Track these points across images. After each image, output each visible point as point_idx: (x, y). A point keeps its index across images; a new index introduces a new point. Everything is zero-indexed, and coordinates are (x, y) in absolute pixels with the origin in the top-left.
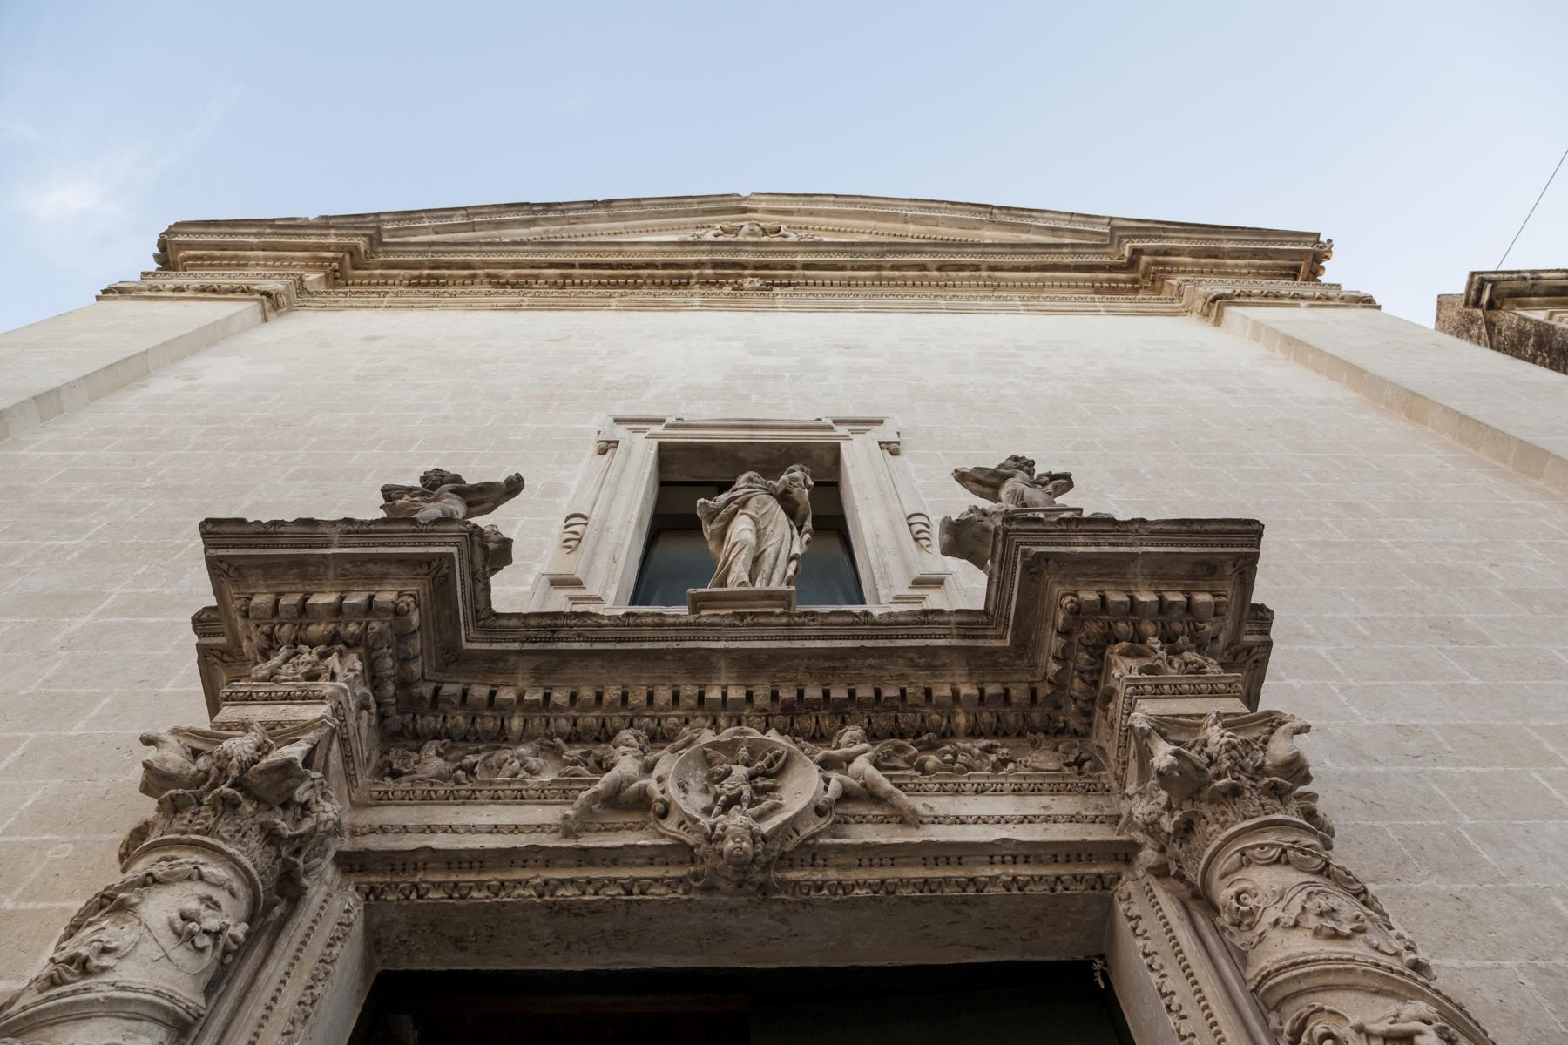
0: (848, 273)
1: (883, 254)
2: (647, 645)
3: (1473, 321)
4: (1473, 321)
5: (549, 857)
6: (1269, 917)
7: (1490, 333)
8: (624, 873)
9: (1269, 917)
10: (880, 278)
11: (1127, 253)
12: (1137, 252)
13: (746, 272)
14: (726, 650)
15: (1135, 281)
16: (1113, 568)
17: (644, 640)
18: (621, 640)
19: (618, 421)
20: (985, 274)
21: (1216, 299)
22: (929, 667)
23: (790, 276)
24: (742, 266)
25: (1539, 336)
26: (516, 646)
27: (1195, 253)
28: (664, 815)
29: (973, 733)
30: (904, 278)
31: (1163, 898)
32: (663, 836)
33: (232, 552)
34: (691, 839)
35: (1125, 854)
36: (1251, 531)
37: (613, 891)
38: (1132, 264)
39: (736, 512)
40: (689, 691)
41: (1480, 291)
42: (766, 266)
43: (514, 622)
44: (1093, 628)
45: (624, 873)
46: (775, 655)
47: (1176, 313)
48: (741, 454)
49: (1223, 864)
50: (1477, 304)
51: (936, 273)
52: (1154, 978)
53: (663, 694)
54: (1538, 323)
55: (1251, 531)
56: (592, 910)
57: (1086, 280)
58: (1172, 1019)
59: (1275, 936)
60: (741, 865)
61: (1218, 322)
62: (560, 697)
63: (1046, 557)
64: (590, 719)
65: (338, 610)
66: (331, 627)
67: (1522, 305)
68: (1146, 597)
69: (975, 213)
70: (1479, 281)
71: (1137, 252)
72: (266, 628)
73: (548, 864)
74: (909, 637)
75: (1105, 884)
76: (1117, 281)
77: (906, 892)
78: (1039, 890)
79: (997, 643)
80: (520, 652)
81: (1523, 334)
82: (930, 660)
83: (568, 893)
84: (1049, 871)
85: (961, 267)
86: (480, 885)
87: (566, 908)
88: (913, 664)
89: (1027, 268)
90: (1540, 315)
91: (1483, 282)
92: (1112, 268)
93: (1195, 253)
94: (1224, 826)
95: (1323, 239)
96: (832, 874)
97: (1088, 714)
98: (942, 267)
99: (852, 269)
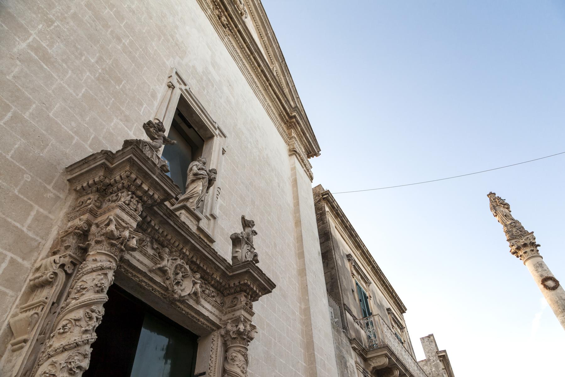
0: (245, 46)
1: (256, 51)
2: (183, 233)
3: (319, 196)
4: (319, 196)
5: (145, 275)
6: (237, 363)
7: (318, 201)
8: (155, 287)
9: (237, 363)
10: (249, 56)
11: (293, 114)
12: (295, 117)
13: (226, 13)
14: (193, 244)
15: (287, 121)
16: (255, 280)
17: (183, 230)
18: (179, 228)
19: (176, 73)
20: (268, 84)
21: (295, 151)
22: (217, 270)
23: (233, 28)
24: (227, 9)
25: (323, 212)
26: (162, 214)
27: (302, 130)
28: (167, 279)
29: (212, 286)
30: (253, 63)
31: (219, 340)
32: (164, 283)
33: (136, 160)
34: (170, 289)
35: (219, 328)
36: (273, 286)
37: (151, 289)
38: (291, 117)
39: (200, 179)
40: (181, 246)
41: (326, 194)
42: (231, 18)
43: (165, 207)
44: (245, 288)
45: (155, 287)
46: (199, 250)
47: (286, 142)
48: (194, 115)
49: (236, 349)
50: (323, 196)
51: (260, 71)
52: (211, 353)
53: (177, 244)
54: (325, 210)
55: (273, 286)
56: (144, 288)
57: (281, 110)
58: (210, 362)
59: (236, 366)
60: (175, 300)
61: (290, 155)
62: (161, 231)
63: (250, 272)
64: (161, 239)
65: (146, 192)
66: (142, 195)
67: (327, 204)
68: (255, 289)
69: (280, 56)
70: (328, 193)
71: (295, 117)
72: (130, 184)
73: (144, 276)
74: (219, 263)
75: (213, 330)
76: (285, 117)
77: (189, 316)
78: (205, 326)
79: (228, 273)
80: (162, 217)
81: (321, 209)
82: (218, 268)
83: (143, 284)
84: (208, 324)
85: (265, 76)
86: (131, 273)
87: (141, 286)
88: (215, 268)
89: (275, 93)
90: (327, 209)
91: (328, 194)
92: (287, 114)
93: (302, 130)
94: (240, 343)
95: (320, 152)
96: (182, 307)
97: (229, 294)
98: (262, 71)
99: (247, 46)
